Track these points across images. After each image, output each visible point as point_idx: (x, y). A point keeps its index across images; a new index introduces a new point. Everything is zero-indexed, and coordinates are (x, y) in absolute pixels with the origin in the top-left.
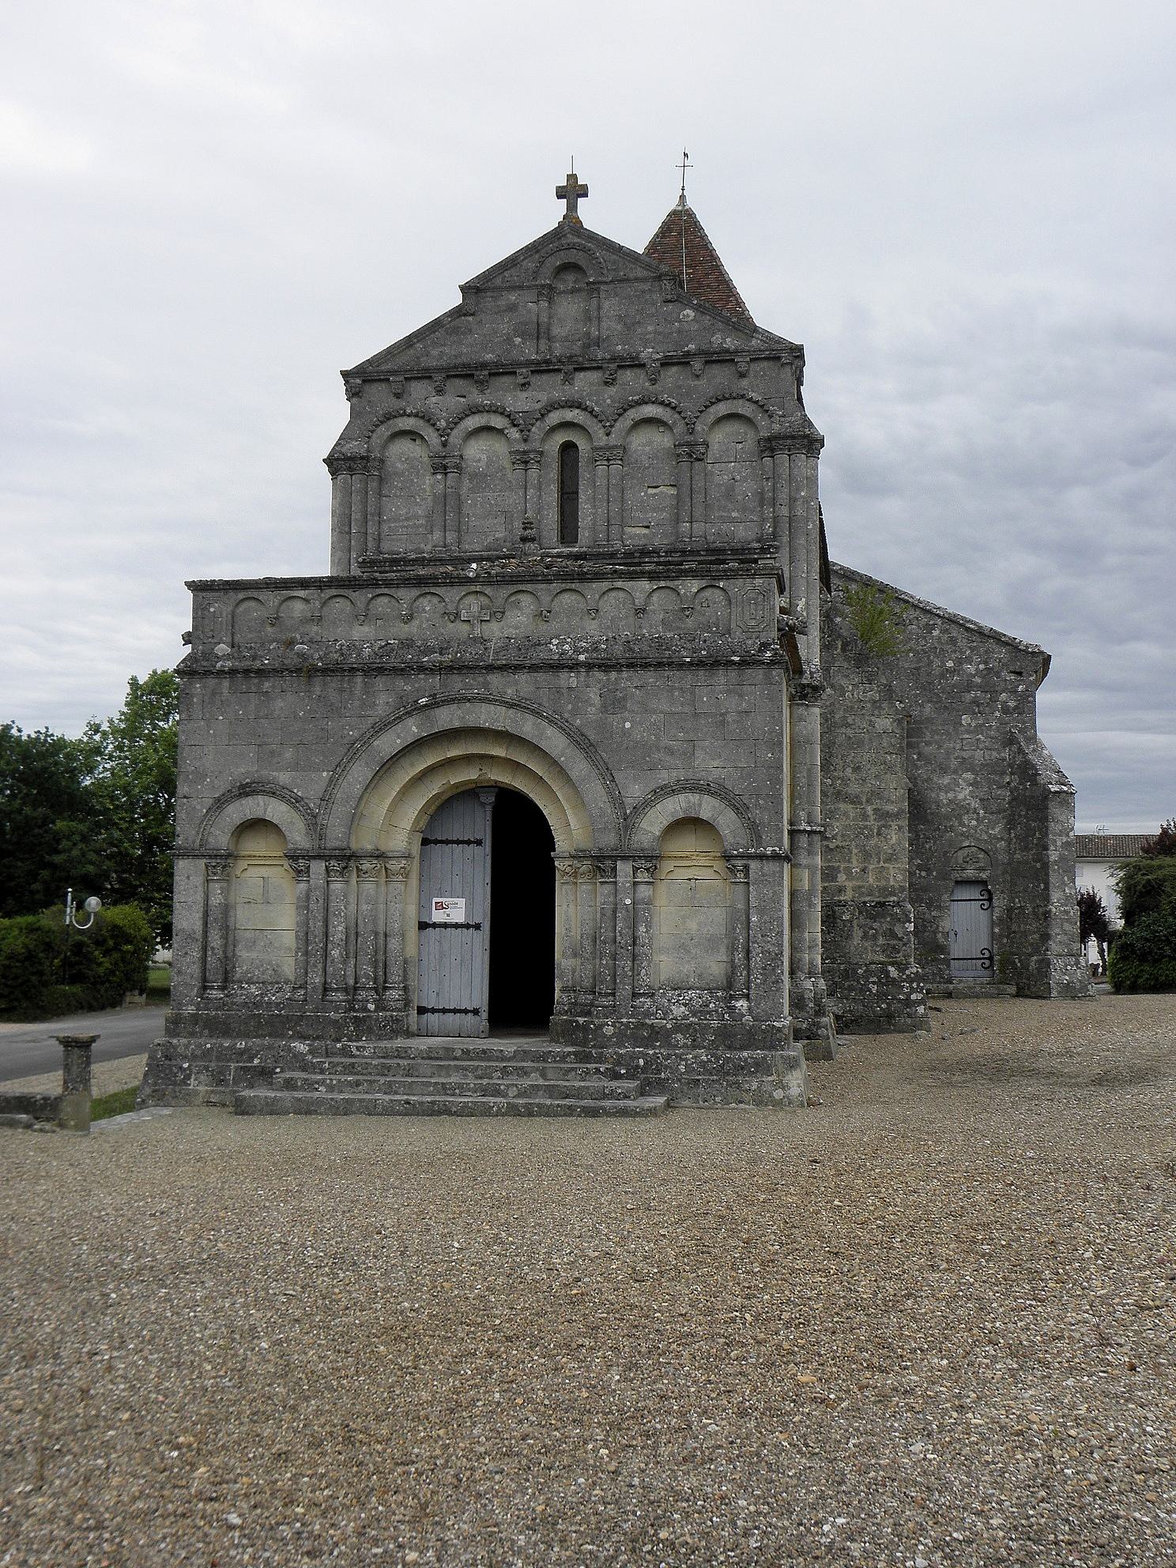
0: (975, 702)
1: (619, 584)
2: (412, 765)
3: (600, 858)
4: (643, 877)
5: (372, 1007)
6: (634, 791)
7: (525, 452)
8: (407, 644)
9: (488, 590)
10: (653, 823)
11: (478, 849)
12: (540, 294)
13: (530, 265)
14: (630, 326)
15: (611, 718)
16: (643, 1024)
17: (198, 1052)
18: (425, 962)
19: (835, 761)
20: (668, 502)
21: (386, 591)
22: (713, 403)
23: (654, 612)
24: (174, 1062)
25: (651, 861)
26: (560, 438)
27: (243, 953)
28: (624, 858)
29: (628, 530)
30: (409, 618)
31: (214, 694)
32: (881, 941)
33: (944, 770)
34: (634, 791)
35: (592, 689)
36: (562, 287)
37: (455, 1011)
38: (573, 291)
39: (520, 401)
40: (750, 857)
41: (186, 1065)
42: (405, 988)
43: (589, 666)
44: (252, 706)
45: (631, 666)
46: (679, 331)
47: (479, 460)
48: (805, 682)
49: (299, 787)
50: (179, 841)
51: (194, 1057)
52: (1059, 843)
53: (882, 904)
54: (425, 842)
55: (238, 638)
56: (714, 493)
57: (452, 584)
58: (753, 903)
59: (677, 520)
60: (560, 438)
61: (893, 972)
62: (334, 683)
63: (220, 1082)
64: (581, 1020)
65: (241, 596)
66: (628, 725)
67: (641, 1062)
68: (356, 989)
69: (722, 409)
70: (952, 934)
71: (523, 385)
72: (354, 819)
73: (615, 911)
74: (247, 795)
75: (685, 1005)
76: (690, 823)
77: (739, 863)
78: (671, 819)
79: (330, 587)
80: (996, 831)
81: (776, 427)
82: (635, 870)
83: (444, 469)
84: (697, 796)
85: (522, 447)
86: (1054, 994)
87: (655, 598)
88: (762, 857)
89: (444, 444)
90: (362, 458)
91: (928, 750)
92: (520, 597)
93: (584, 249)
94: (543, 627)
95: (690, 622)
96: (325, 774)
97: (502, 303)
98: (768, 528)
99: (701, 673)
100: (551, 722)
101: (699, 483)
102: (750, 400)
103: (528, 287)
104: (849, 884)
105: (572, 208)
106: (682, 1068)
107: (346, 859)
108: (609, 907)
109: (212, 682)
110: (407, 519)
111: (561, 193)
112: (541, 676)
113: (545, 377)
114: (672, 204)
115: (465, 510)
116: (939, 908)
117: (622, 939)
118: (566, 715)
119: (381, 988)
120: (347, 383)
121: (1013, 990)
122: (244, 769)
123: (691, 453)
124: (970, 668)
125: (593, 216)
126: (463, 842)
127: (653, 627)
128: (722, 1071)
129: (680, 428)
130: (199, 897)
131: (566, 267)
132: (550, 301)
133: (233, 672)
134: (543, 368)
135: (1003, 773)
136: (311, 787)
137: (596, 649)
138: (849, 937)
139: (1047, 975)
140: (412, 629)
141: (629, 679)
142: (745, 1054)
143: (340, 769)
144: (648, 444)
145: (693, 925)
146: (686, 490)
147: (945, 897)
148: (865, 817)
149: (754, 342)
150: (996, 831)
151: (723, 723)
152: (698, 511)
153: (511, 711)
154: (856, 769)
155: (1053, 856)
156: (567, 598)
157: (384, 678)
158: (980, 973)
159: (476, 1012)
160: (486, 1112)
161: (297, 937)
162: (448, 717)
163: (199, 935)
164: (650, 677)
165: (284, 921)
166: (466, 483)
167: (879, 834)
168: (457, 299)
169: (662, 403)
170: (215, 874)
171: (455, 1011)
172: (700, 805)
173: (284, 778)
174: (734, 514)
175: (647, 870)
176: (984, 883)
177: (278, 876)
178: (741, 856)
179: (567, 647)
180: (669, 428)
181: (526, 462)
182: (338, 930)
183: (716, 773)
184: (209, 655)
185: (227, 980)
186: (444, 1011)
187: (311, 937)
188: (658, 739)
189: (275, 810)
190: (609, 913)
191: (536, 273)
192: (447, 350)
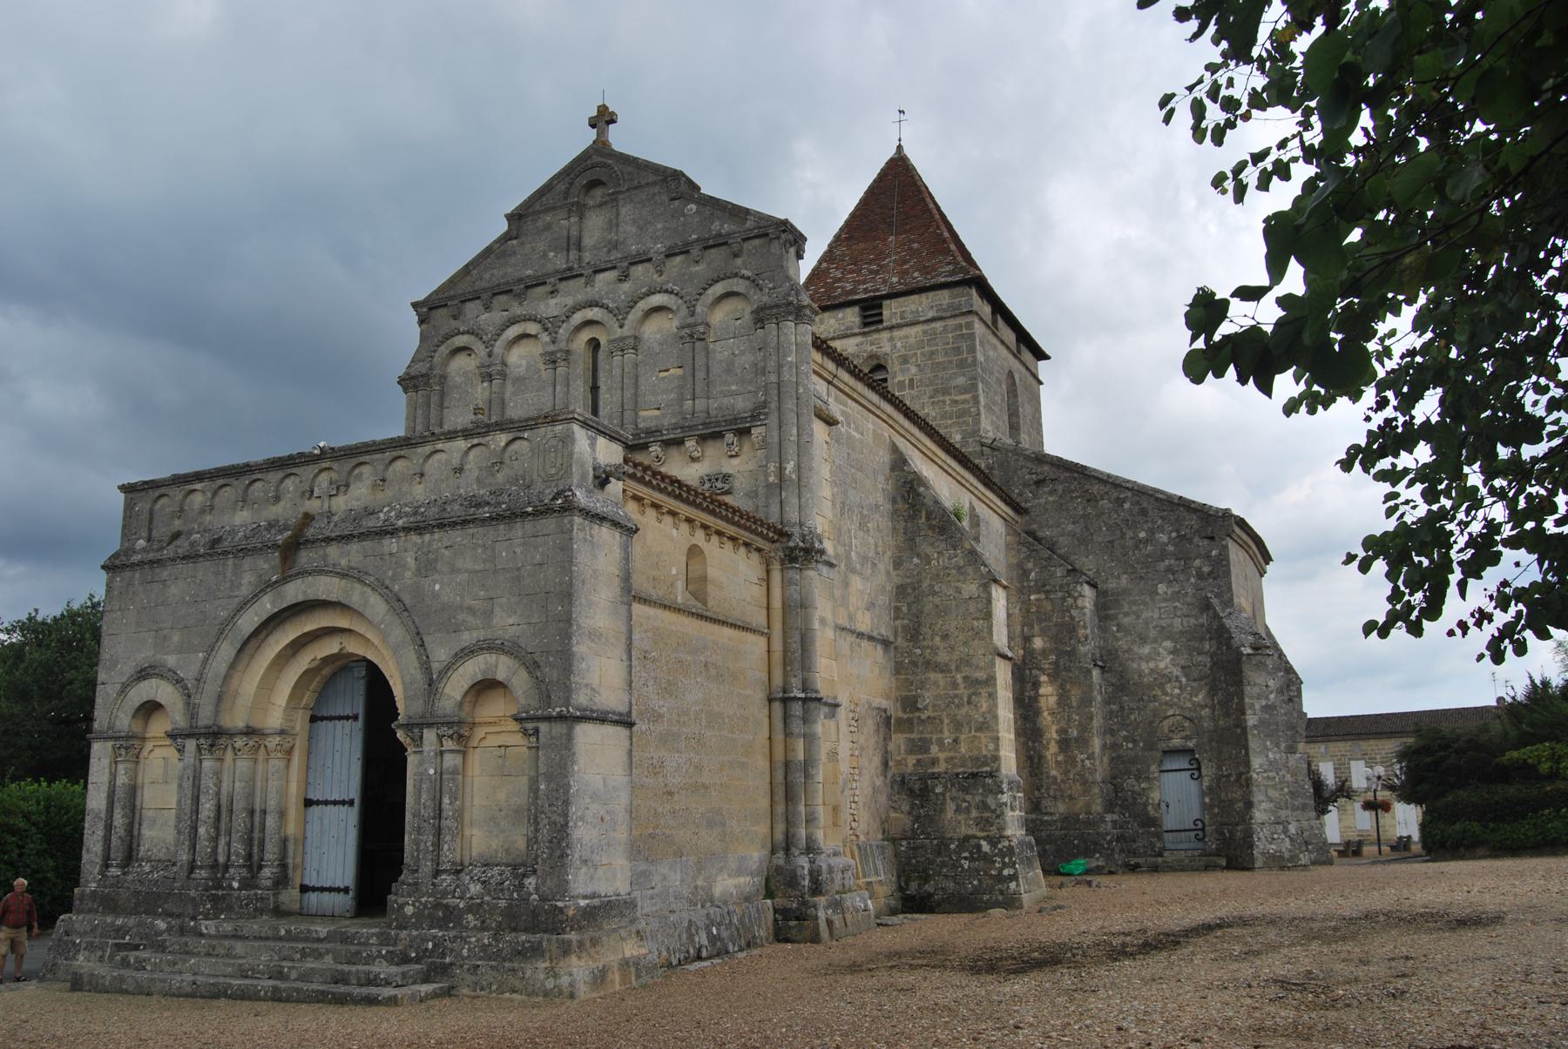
0: (1169, 570)
2: (277, 642)
4: (449, 744)
5: (235, 885)
7: (552, 353)
10: (455, 687)
12: (570, 211)
13: (562, 187)
18: (309, 840)
19: (924, 630)
27: (147, 833)
28: (430, 725)
29: (642, 413)
30: (277, 499)
32: (974, 813)
33: (1143, 640)
34: (440, 654)
36: (591, 203)
37: (331, 890)
38: (600, 205)
45: (441, 526)
48: (791, 544)
50: (96, 725)
52: (1257, 707)
53: (974, 775)
56: (716, 370)
58: (542, 770)
59: (681, 400)
60: (586, 335)
61: (986, 847)
66: (437, 587)
67: (430, 945)
69: (719, 289)
70: (1163, 806)
76: (486, 687)
78: (470, 683)
80: (1200, 698)
81: (765, 299)
82: (440, 738)
85: (552, 348)
86: (1258, 864)
88: (548, 719)
91: (1126, 621)
97: (540, 224)
102: (743, 277)
104: (942, 756)
105: (602, 134)
109: (127, 574)
113: (571, 283)
114: (891, 152)
116: (1148, 779)
119: (253, 865)
121: (1224, 862)
122: (143, 656)
123: (694, 336)
124: (1163, 538)
125: (621, 139)
127: (469, 485)
129: (684, 311)
135: (1202, 639)
138: (943, 810)
139: (1251, 846)
141: (440, 540)
143: (211, 650)
144: (657, 330)
147: (1153, 768)
148: (955, 685)
150: (1200, 698)
151: (518, 579)
154: (945, 637)
155: (1251, 720)
156: (399, 464)
158: (1192, 845)
159: (346, 890)
162: (294, 592)
164: (456, 536)
166: (509, 388)
167: (969, 703)
168: (503, 227)
169: (666, 291)
171: (331, 890)
173: (171, 660)
175: (451, 737)
176: (1191, 751)
182: (207, 808)
183: (512, 631)
185: (130, 857)
186: (322, 889)
188: (462, 598)
191: (567, 194)
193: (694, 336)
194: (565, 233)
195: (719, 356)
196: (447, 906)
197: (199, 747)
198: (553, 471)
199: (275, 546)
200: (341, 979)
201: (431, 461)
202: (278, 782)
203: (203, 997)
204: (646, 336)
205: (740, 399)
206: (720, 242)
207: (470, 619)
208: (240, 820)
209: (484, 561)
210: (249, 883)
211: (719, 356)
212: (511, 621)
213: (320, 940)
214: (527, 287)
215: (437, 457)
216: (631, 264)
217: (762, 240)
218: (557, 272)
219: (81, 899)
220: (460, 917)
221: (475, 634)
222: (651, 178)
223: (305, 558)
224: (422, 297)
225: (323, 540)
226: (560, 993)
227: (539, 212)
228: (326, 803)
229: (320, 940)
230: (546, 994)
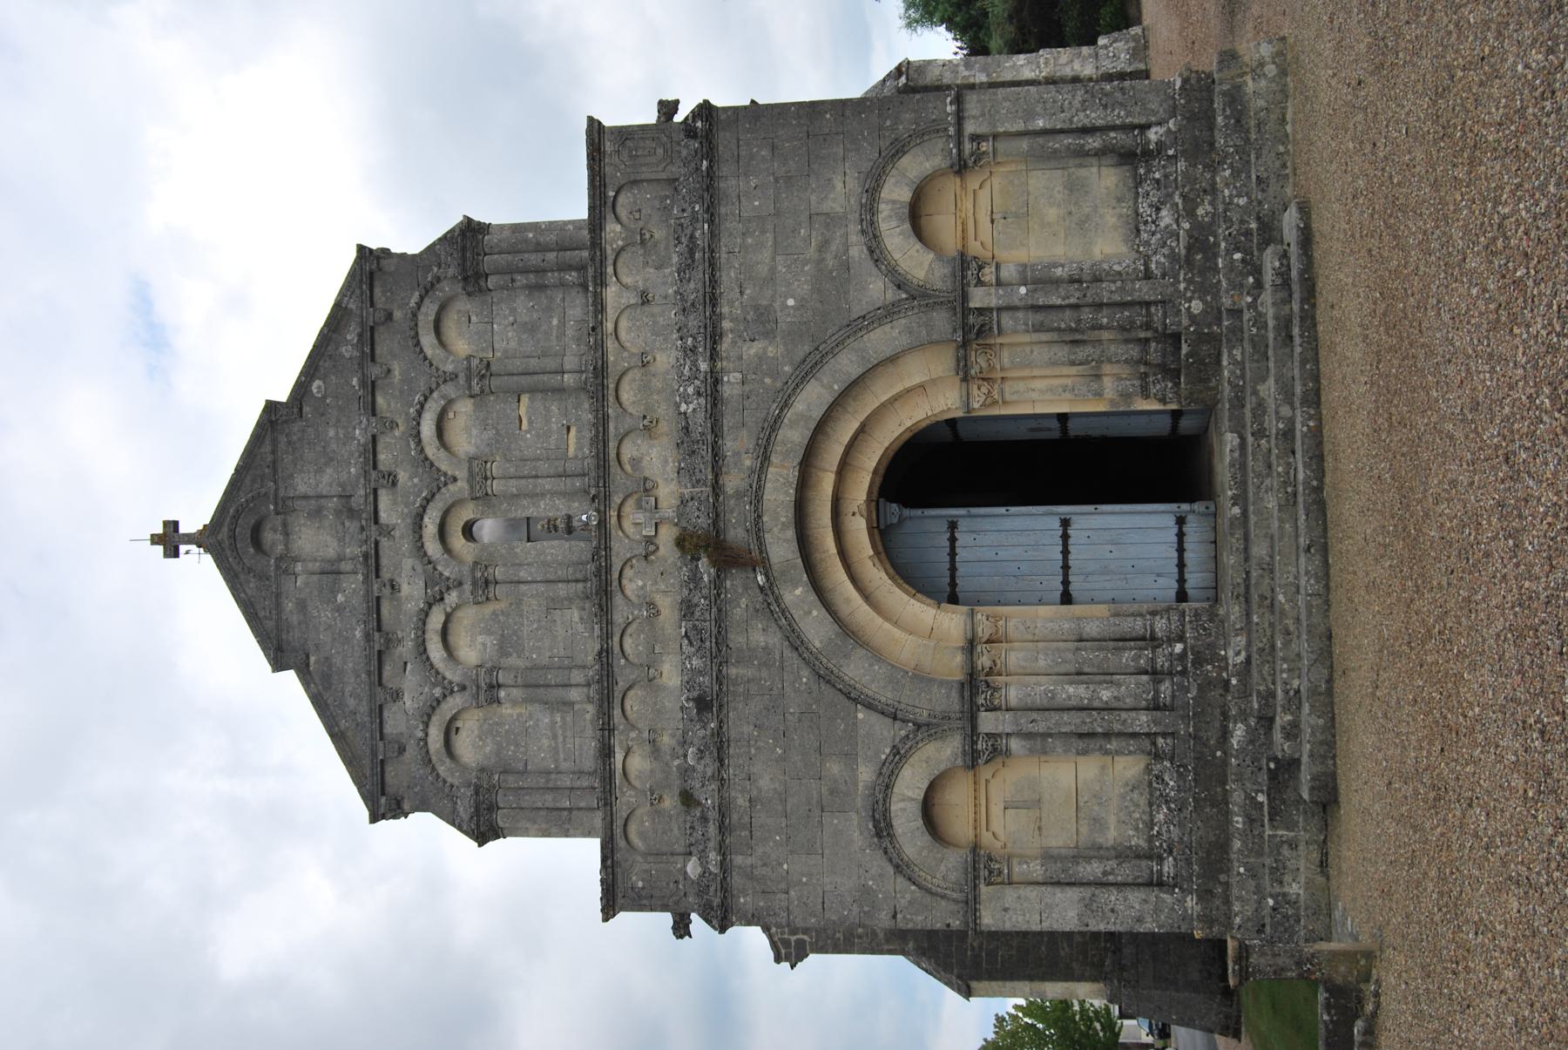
1: (610, 326)
2: (848, 601)
3: (966, 328)
5: (1179, 648)
6: (877, 290)
7: (474, 583)
8: (687, 609)
9: (617, 499)
11: (963, 525)
12: (286, 572)
13: (252, 586)
15: (782, 326)
17: (1252, 883)
20: (538, 404)
21: (616, 639)
22: (422, 351)
23: (646, 280)
24: (1267, 920)
25: (965, 266)
27: (1111, 836)
28: (965, 297)
29: (571, 452)
31: (750, 877)
34: (877, 290)
35: (747, 357)
37: (1181, 550)
38: (287, 534)
39: (412, 591)
40: (960, 132)
41: (1271, 902)
42: (1153, 613)
43: (714, 356)
47: (484, 645)
50: (956, 924)
51: (1259, 890)
54: (953, 599)
55: (679, 848)
57: (608, 548)
58: (1019, 126)
59: (560, 390)
64: (1185, 349)
65: (622, 843)
66: (791, 302)
67: (1237, 256)
68: (1154, 672)
71: (393, 587)
72: (921, 678)
73: (1036, 308)
74: (890, 826)
75: (1158, 210)
76: (916, 216)
77: (968, 147)
78: (913, 239)
82: (980, 283)
83: (494, 687)
84: (882, 206)
85: (467, 587)
87: (627, 280)
88: (960, 119)
89: (463, 688)
90: (477, 793)
92: (625, 458)
93: (236, 518)
94: (664, 427)
95: (659, 234)
96: (860, 716)
97: (295, 619)
98: (570, 277)
99: (723, 210)
100: (786, 405)
101: (517, 364)
102: (419, 305)
103: (278, 586)
105: (189, 539)
106: (1242, 201)
107: (975, 686)
108: (1033, 318)
109: (736, 880)
110: (555, 737)
111: (172, 552)
112: (727, 422)
113: (384, 561)
115: (545, 661)
117: (1073, 309)
118: (779, 384)
119: (1151, 640)
120: (384, 817)
122: (854, 829)
123: (482, 379)
125: (195, 519)
127: (663, 282)
129: (449, 390)
130: (1032, 893)
131: (256, 541)
132: (296, 560)
133: (723, 850)
134: (373, 562)
136: (880, 733)
137: (693, 350)
140: (667, 606)
141: (731, 303)
142: (1219, 119)
143: (854, 697)
145: (1052, 213)
146: (525, 381)
149: (352, 306)
151: (789, 179)
152: (551, 364)
153: (773, 459)
156: (626, 396)
157: (731, 636)
159: (1181, 521)
160: (1317, 436)
161: (1084, 752)
162: (781, 548)
163: (1087, 892)
165: (1064, 776)
166: (513, 661)
168: (290, 677)
169: (419, 413)
170: (1000, 873)
171: (1181, 550)
172: (894, 202)
173: (866, 774)
174: (555, 322)
175: (980, 268)
177: (1004, 782)
178: (959, 144)
179: (690, 390)
180: (450, 402)
181: (487, 582)
182: (1075, 692)
183: (853, 183)
184: (702, 888)
186: (1181, 565)
187: (1085, 729)
189: (910, 784)
190: (1039, 317)
191: (263, 577)
192: (348, 689)
193: (482, 379)
194: (315, 578)
195: (513, 344)
196: (1189, 248)
197: (993, 709)
198: (660, 151)
199: (717, 583)
200: (1285, 283)
202: (1033, 646)
203: (1325, 530)
204: (472, 450)
205: (570, 312)
206: (369, 337)
208: (1091, 656)
209: (763, 232)
211: (513, 344)
212: (839, 185)
213: (1243, 439)
214: (379, 629)
215: (623, 335)
216: (375, 467)
217: (377, 284)
218: (366, 577)
221: (853, 238)
222: (267, 448)
223: (736, 534)
224: (366, 813)
225: (716, 496)
226: (1280, 54)
227: (279, 620)
228: (1066, 567)
229: (1243, 439)
230: (1283, 73)
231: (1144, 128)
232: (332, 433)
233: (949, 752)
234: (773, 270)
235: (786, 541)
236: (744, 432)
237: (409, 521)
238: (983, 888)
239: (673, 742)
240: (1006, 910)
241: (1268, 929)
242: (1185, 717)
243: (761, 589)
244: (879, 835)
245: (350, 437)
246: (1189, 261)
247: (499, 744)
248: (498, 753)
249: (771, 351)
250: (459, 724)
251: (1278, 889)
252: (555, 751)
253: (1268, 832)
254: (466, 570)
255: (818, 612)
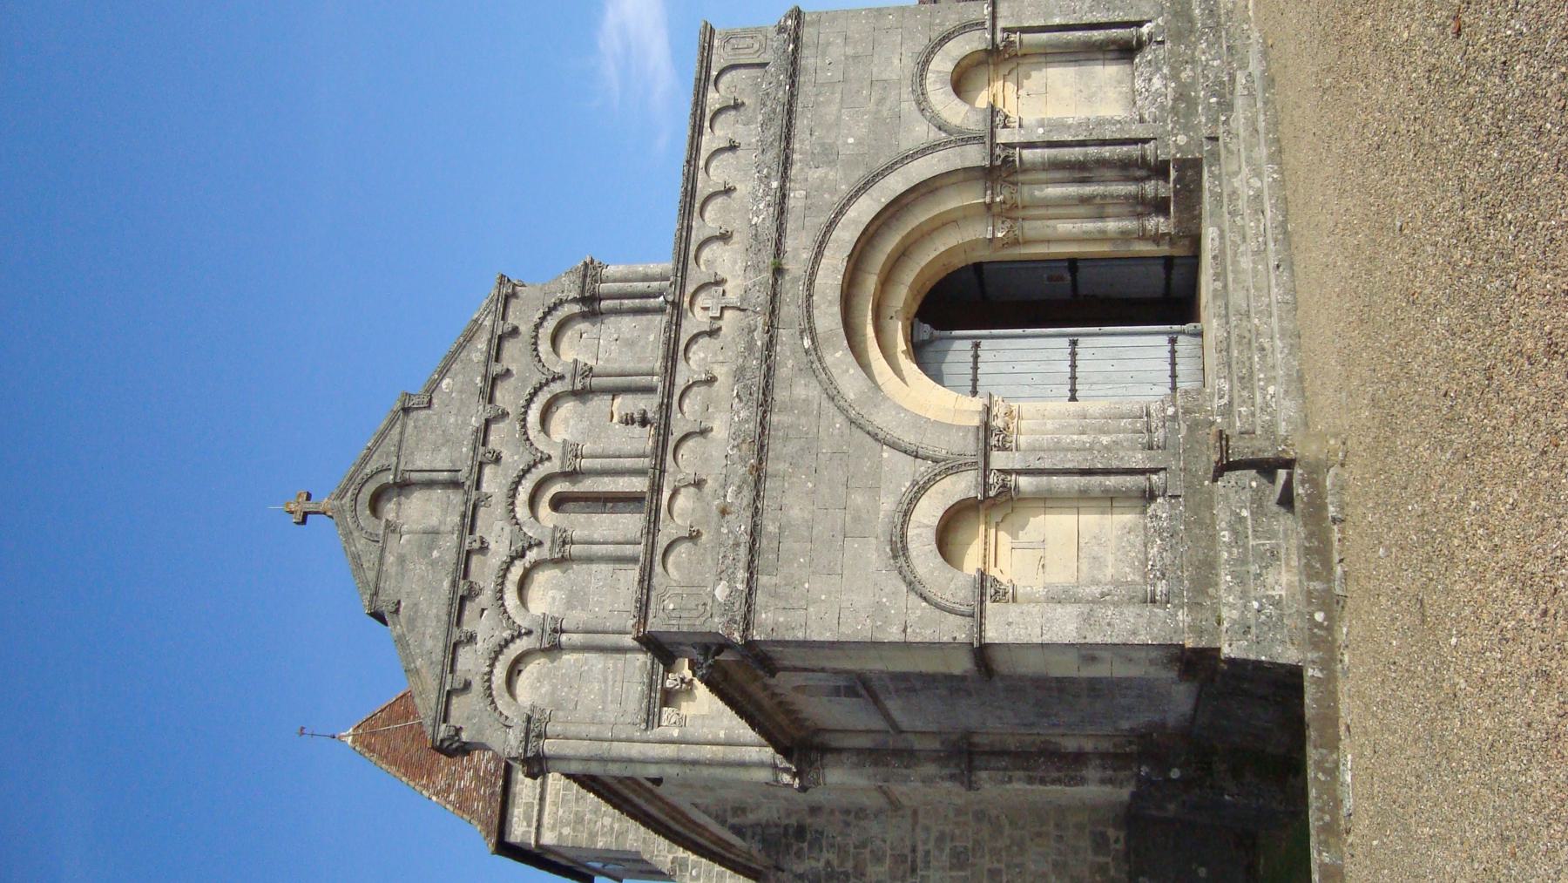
7: (553, 542)
14: (447, 440)
16: (1173, 108)
17: (1238, 589)
24: (1252, 622)
26: (544, 509)
34: (921, 132)
37: (1173, 364)
40: (994, 26)
43: (784, 177)
44: (796, 546)
46: (461, 392)
47: (554, 598)
49: (899, 486)
62: (775, 447)
63: (1274, 555)
67: (1213, 100)
74: (905, 548)
77: (999, 36)
79: (663, 460)
96: (885, 455)
106: (1216, 63)
109: (760, 598)
110: (606, 681)
113: (479, 523)
122: (874, 553)
126: (976, 363)
128: (1216, 28)
130: (1035, 609)
136: (901, 472)
141: (802, 141)
151: (856, 57)
159: (1173, 341)
164: (801, 124)
171: (1173, 364)
173: (887, 505)
178: (993, 34)
186: (1174, 376)
196: (1175, 100)
197: (1003, 448)
201: (711, 171)
207: (888, 104)
210: (1160, 207)
212: (896, 61)
219: (1200, 632)
220: (1184, 85)
228: (1073, 378)
231: (1140, 24)
232: (452, 420)
233: (963, 485)
234: (839, 118)
235: (832, 315)
236: (804, 233)
237: (505, 490)
238: (989, 604)
239: (716, 485)
240: (1010, 624)
241: (1253, 630)
242: (1176, 455)
243: (807, 352)
244: (895, 557)
245: (466, 423)
246: (1174, 110)
247: (554, 687)
248: (553, 693)
249: (831, 175)
250: (521, 667)
251: (1261, 591)
252: (605, 693)
253: (1252, 542)
254: (548, 533)
255: (854, 370)
